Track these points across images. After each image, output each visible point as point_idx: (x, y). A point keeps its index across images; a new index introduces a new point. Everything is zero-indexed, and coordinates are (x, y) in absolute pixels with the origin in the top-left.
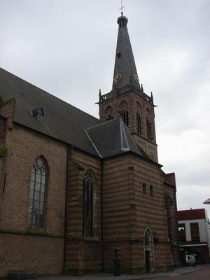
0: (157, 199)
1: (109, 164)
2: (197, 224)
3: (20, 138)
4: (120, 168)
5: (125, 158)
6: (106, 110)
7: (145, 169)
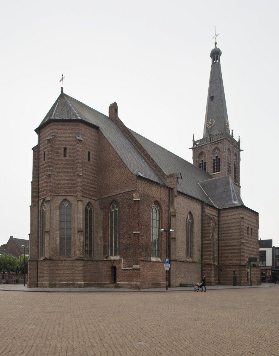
2: (265, 252)
4: (233, 217)
6: (199, 156)
7: (249, 217)
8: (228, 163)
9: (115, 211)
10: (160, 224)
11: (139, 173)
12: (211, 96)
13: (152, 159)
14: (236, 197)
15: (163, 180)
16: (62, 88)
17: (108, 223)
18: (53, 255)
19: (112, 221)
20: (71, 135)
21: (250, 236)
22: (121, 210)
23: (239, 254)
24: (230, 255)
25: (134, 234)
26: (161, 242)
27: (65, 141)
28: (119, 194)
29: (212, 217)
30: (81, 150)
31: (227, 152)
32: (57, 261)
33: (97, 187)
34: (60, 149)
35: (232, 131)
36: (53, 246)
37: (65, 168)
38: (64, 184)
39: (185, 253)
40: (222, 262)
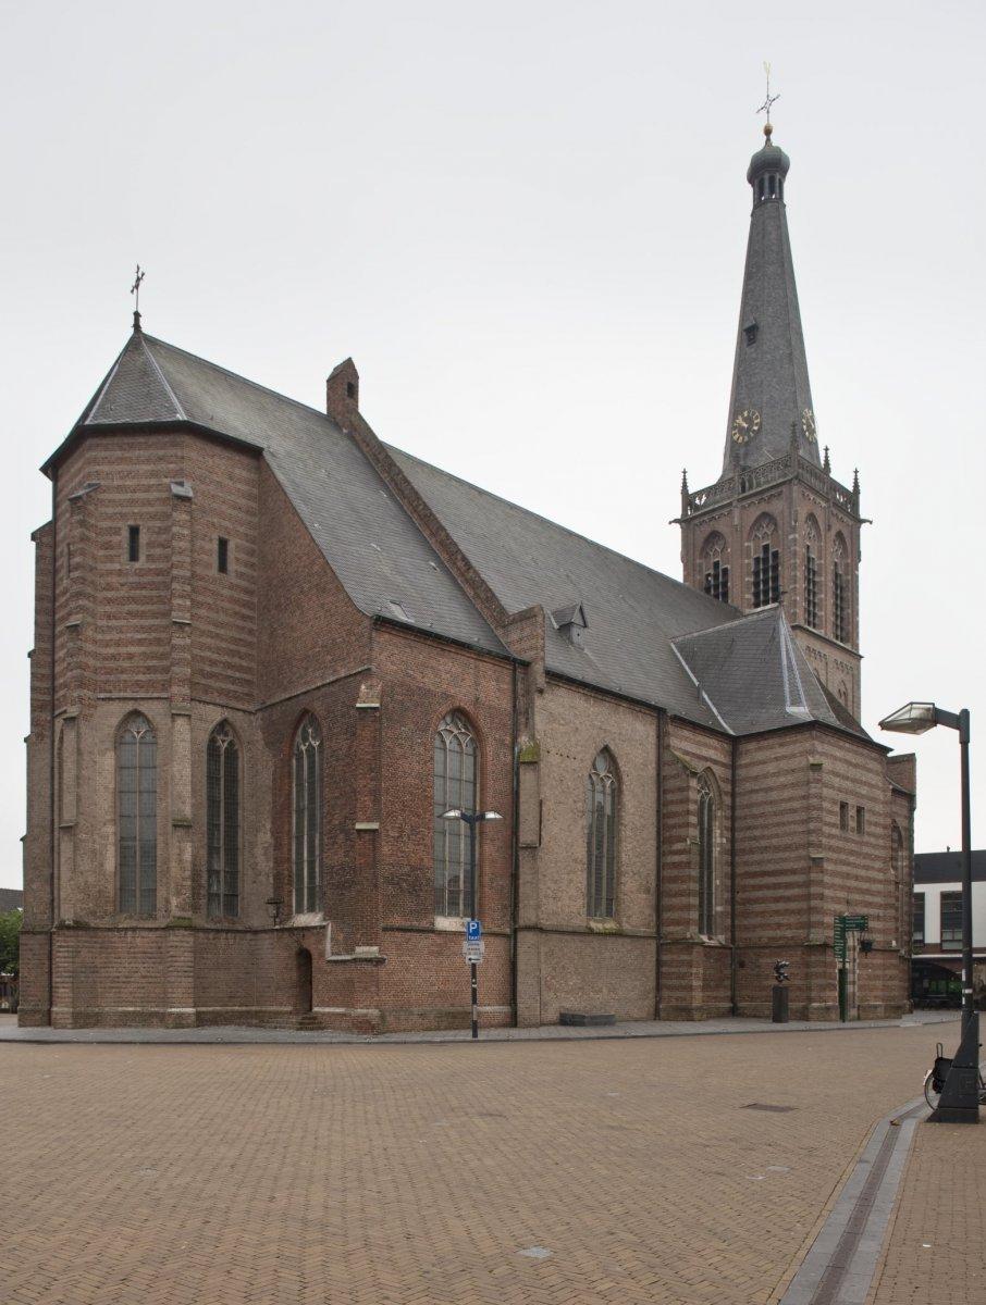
0: (872, 840)
1: (753, 753)
3: (561, 710)
4: (783, 765)
5: (799, 737)
6: (703, 549)
8: (809, 569)
9: (311, 749)
10: (478, 794)
11: (394, 607)
12: (747, 325)
13: (464, 559)
14: (801, 692)
15: (499, 632)
16: (137, 315)
17: (290, 794)
18: (93, 913)
19: (300, 785)
20: (153, 481)
21: (854, 836)
22: (326, 744)
23: (803, 905)
24: (773, 906)
25: (359, 831)
26: (481, 860)
27: (132, 502)
28: (318, 688)
29: (700, 766)
30: (186, 532)
31: (804, 528)
32: (105, 934)
33: (254, 665)
34: (117, 531)
35: (827, 449)
36: (91, 879)
37: (134, 600)
38: (130, 657)
39: (581, 902)
40: (745, 935)
